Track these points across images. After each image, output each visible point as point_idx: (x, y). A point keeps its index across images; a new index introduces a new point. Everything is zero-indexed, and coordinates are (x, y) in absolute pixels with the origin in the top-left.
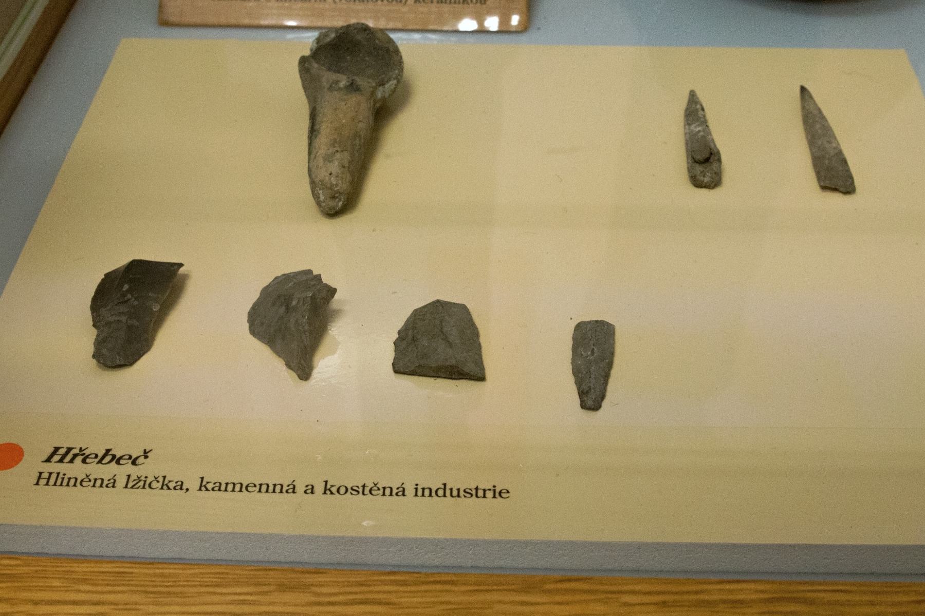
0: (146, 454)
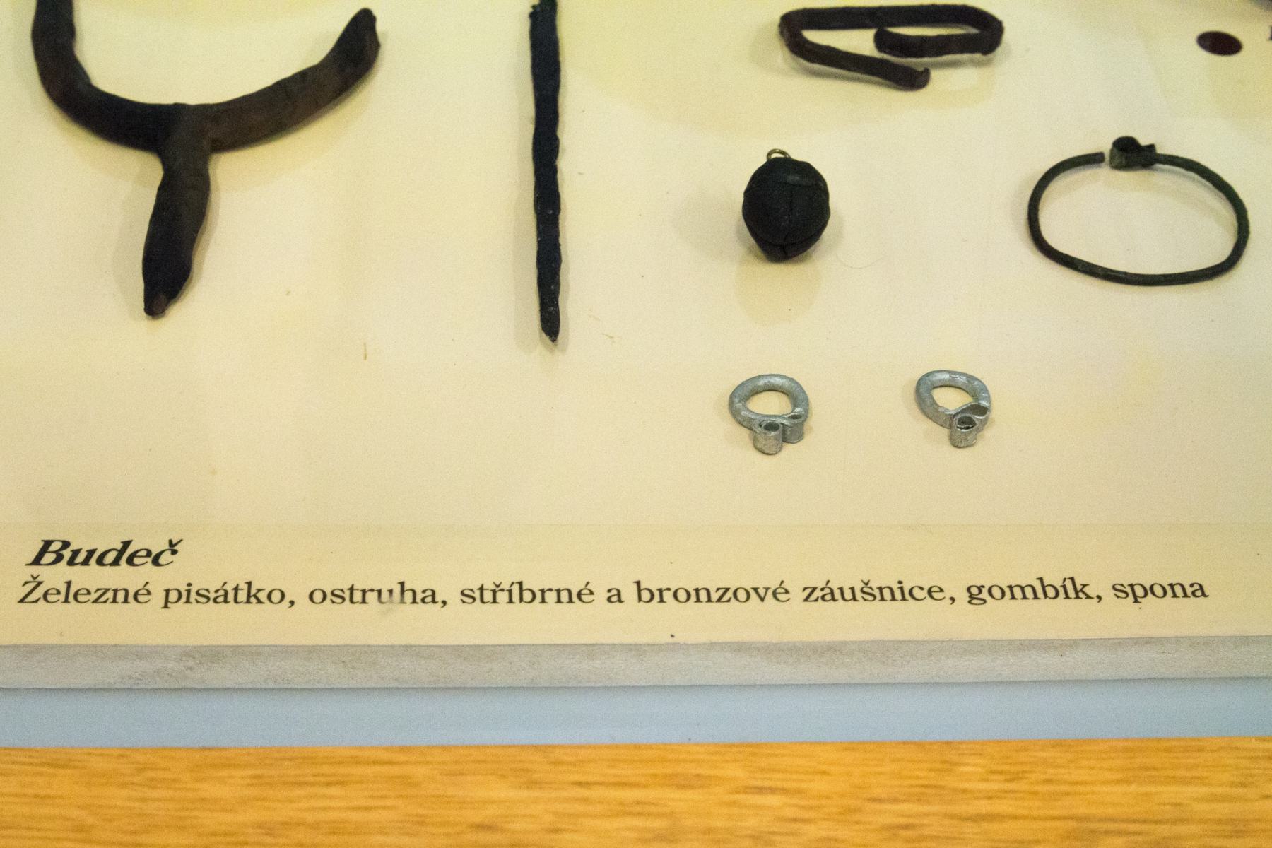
0: (173, 548)
